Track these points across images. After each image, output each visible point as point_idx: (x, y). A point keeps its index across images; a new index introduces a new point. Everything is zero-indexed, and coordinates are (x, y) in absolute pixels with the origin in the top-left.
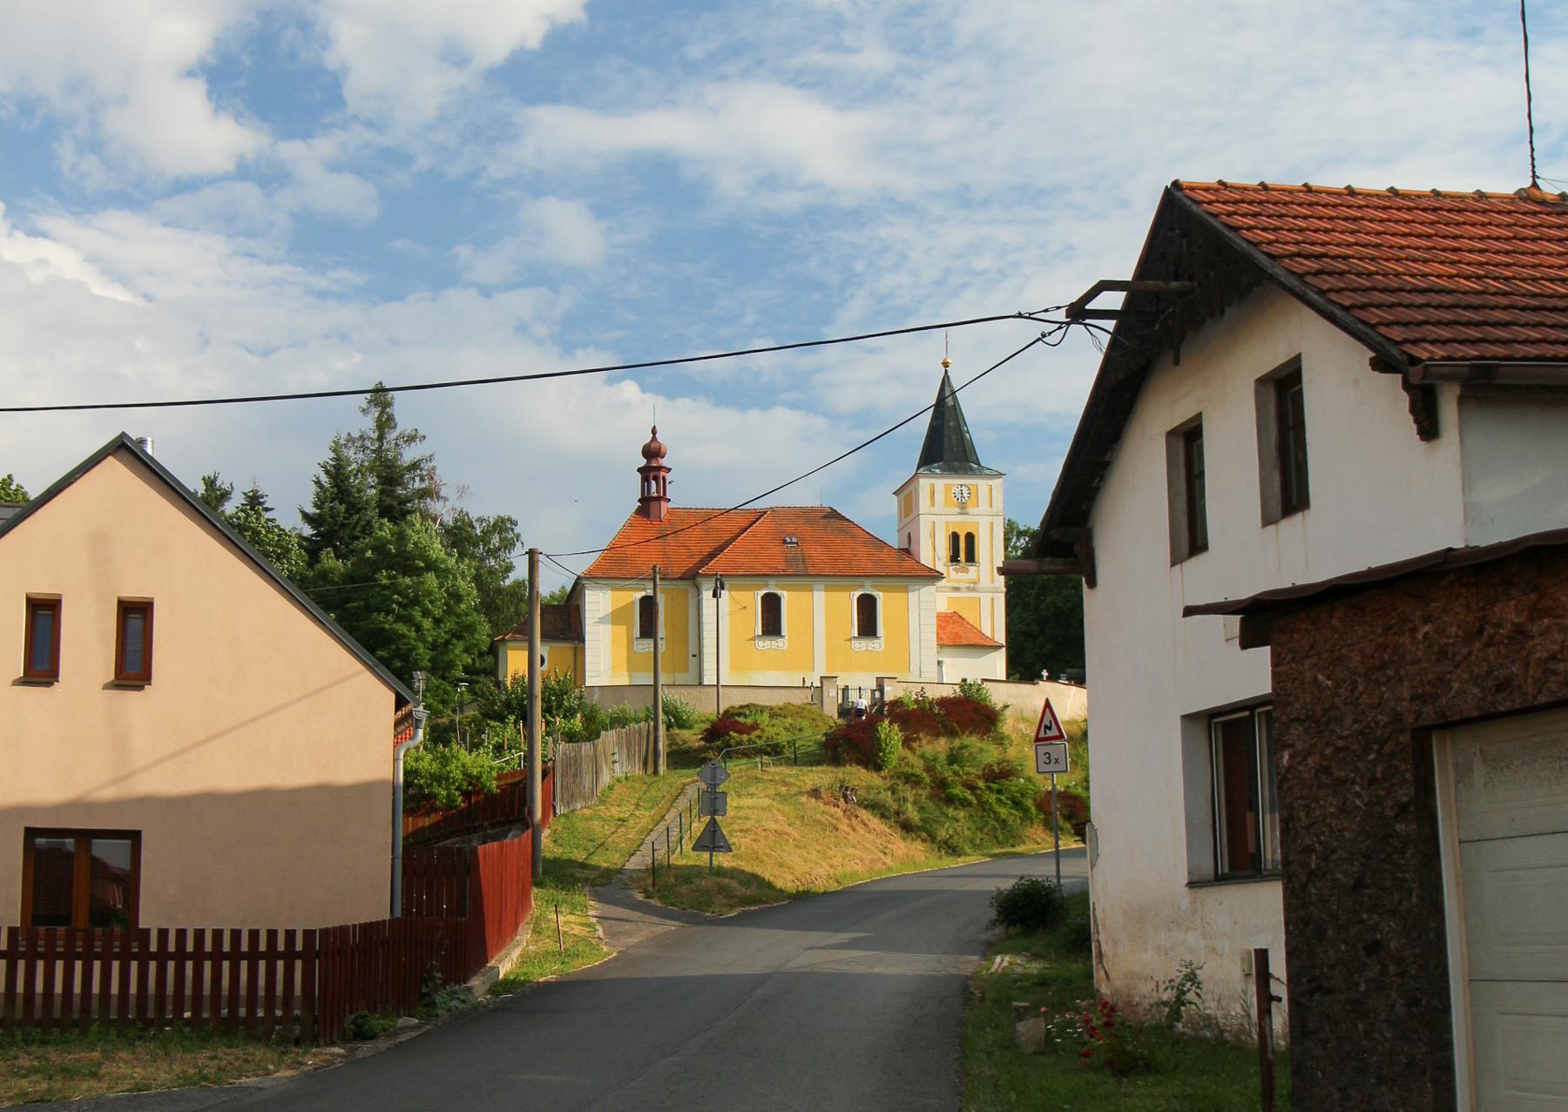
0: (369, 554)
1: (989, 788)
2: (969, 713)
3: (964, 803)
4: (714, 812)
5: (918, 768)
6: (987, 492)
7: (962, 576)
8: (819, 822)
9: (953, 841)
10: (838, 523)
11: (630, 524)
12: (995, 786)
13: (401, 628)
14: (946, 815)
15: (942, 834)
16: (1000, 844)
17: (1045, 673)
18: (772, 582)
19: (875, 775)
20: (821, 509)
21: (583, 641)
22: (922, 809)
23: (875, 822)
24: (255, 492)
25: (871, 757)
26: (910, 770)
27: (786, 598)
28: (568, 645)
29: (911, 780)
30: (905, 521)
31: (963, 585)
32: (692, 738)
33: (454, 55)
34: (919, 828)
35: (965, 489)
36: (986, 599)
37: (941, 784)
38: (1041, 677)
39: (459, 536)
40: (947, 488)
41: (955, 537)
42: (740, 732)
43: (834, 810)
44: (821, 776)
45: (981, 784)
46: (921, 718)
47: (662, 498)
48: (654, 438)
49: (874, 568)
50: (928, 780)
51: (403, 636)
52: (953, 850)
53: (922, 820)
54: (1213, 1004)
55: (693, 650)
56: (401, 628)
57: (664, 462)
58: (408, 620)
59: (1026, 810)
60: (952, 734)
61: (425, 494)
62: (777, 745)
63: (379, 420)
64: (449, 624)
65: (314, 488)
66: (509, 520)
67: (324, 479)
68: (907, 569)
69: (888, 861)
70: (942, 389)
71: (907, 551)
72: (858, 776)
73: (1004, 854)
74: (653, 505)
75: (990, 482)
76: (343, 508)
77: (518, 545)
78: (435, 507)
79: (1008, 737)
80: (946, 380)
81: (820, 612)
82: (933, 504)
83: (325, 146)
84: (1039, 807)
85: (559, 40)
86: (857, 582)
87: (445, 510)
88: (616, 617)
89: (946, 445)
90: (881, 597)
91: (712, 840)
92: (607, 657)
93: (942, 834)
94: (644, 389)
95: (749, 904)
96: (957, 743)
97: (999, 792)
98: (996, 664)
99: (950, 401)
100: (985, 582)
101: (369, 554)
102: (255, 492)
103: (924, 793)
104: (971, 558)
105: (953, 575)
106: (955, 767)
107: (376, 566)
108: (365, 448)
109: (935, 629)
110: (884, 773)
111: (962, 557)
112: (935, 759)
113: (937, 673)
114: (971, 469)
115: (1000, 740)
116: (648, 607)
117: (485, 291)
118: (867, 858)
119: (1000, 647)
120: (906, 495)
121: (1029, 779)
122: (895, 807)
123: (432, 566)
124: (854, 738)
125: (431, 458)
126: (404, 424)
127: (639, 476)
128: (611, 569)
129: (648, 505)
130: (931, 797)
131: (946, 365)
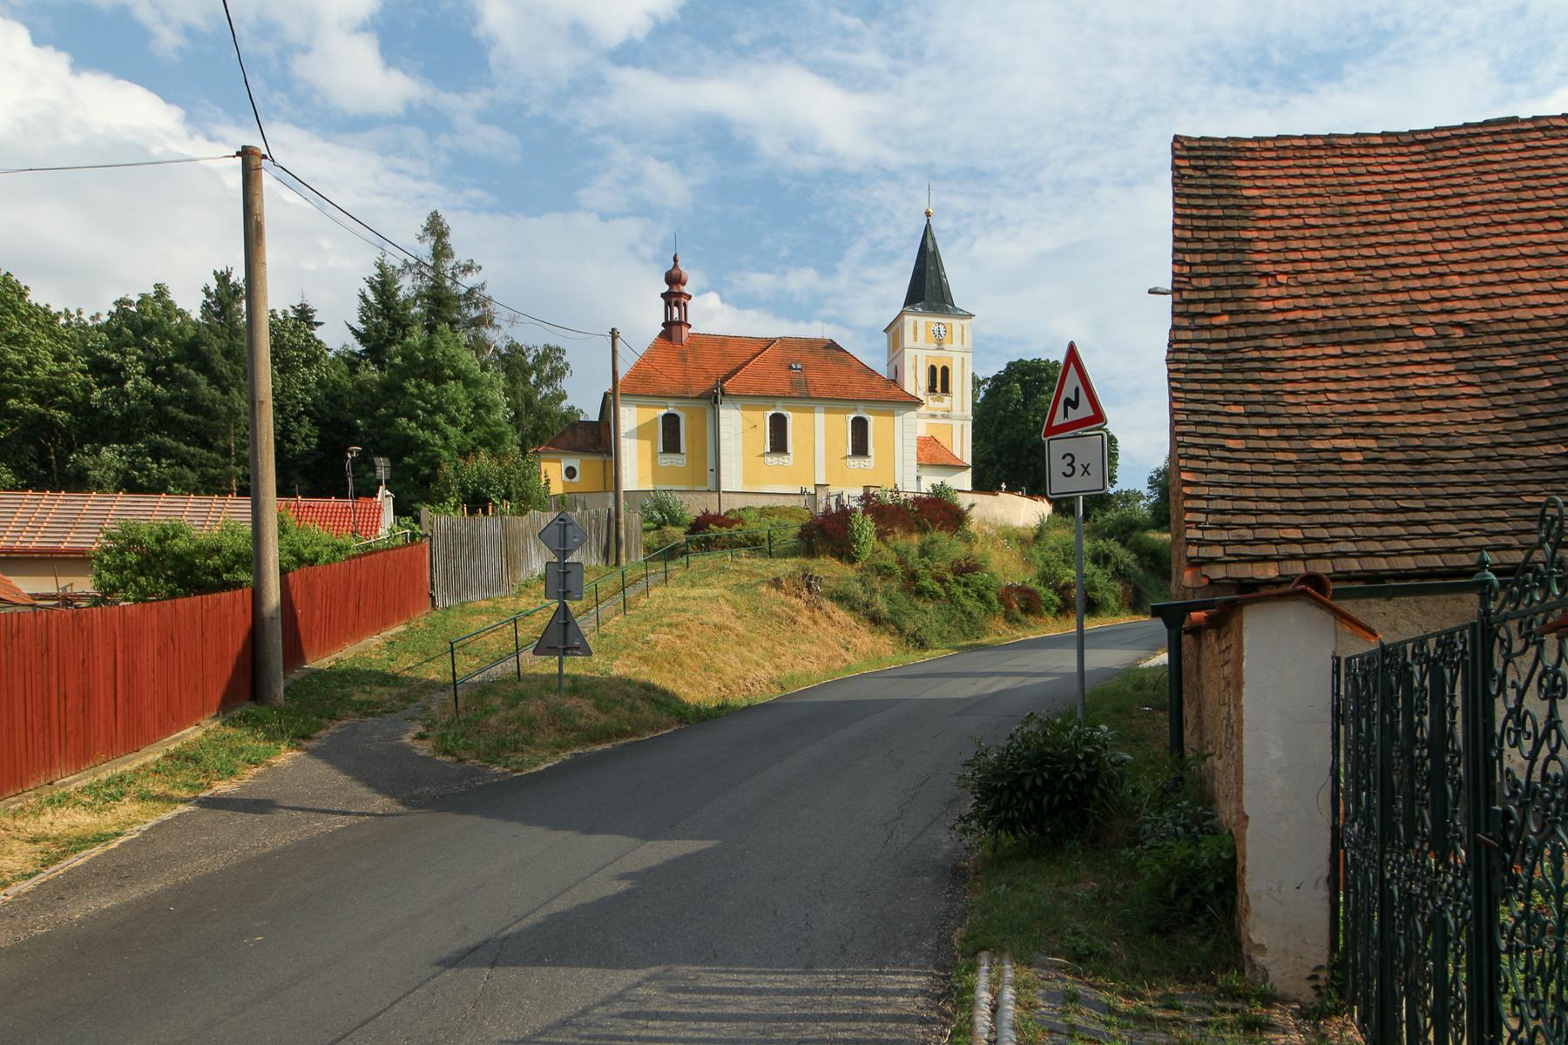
0: (398, 360)
1: (958, 582)
2: (938, 512)
3: (934, 596)
4: (565, 594)
5: (890, 559)
7: (938, 404)
8: (773, 614)
9: (922, 634)
10: (836, 353)
11: (655, 346)
12: (963, 580)
13: (424, 435)
14: (916, 608)
15: (910, 626)
18: (779, 403)
20: (822, 341)
22: (891, 600)
23: (840, 615)
24: (304, 306)
26: (882, 563)
27: (792, 418)
29: (884, 572)
31: (939, 413)
32: (678, 534)
33: (579, 33)
36: (957, 425)
37: (913, 577)
39: (512, 362)
40: (927, 324)
41: (933, 369)
42: (720, 526)
43: (794, 601)
44: (785, 567)
45: (950, 577)
46: (889, 514)
47: (682, 323)
48: (675, 266)
50: (899, 572)
51: (425, 442)
52: (922, 645)
55: (711, 464)
56: (424, 435)
57: (686, 289)
58: (434, 428)
59: (989, 603)
61: (478, 322)
62: (757, 538)
63: (434, 248)
64: (479, 432)
65: (357, 303)
66: (558, 349)
67: (371, 297)
69: (850, 657)
70: (925, 236)
72: (828, 568)
73: (970, 646)
76: (387, 323)
78: (490, 334)
79: (974, 535)
80: (928, 228)
81: (819, 432)
82: (915, 340)
83: (477, 100)
84: (1001, 600)
85: (661, 30)
86: (851, 405)
87: (497, 338)
88: (642, 432)
90: (872, 420)
91: (562, 637)
92: (637, 465)
93: (910, 626)
94: (723, 301)
95: (594, 741)
96: (928, 537)
97: (966, 585)
98: (964, 480)
99: (930, 246)
100: (956, 411)
101: (398, 360)
102: (304, 306)
103: (895, 585)
105: (931, 404)
106: (926, 559)
107: (404, 373)
108: (422, 275)
110: (859, 565)
113: (912, 481)
115: (968, 539)
116: (671, 422)
117: (604, 217)
118: (825, 655)
120: (894, 330)
121: (992, 575)
122: (865, 599)
123: (459, 376)
124: (827, 532)
125: (483, 287)
126: (461, 256)
128: (638, 386)
129: (671, 329)
130: (903, 590)
131: (928, 214)
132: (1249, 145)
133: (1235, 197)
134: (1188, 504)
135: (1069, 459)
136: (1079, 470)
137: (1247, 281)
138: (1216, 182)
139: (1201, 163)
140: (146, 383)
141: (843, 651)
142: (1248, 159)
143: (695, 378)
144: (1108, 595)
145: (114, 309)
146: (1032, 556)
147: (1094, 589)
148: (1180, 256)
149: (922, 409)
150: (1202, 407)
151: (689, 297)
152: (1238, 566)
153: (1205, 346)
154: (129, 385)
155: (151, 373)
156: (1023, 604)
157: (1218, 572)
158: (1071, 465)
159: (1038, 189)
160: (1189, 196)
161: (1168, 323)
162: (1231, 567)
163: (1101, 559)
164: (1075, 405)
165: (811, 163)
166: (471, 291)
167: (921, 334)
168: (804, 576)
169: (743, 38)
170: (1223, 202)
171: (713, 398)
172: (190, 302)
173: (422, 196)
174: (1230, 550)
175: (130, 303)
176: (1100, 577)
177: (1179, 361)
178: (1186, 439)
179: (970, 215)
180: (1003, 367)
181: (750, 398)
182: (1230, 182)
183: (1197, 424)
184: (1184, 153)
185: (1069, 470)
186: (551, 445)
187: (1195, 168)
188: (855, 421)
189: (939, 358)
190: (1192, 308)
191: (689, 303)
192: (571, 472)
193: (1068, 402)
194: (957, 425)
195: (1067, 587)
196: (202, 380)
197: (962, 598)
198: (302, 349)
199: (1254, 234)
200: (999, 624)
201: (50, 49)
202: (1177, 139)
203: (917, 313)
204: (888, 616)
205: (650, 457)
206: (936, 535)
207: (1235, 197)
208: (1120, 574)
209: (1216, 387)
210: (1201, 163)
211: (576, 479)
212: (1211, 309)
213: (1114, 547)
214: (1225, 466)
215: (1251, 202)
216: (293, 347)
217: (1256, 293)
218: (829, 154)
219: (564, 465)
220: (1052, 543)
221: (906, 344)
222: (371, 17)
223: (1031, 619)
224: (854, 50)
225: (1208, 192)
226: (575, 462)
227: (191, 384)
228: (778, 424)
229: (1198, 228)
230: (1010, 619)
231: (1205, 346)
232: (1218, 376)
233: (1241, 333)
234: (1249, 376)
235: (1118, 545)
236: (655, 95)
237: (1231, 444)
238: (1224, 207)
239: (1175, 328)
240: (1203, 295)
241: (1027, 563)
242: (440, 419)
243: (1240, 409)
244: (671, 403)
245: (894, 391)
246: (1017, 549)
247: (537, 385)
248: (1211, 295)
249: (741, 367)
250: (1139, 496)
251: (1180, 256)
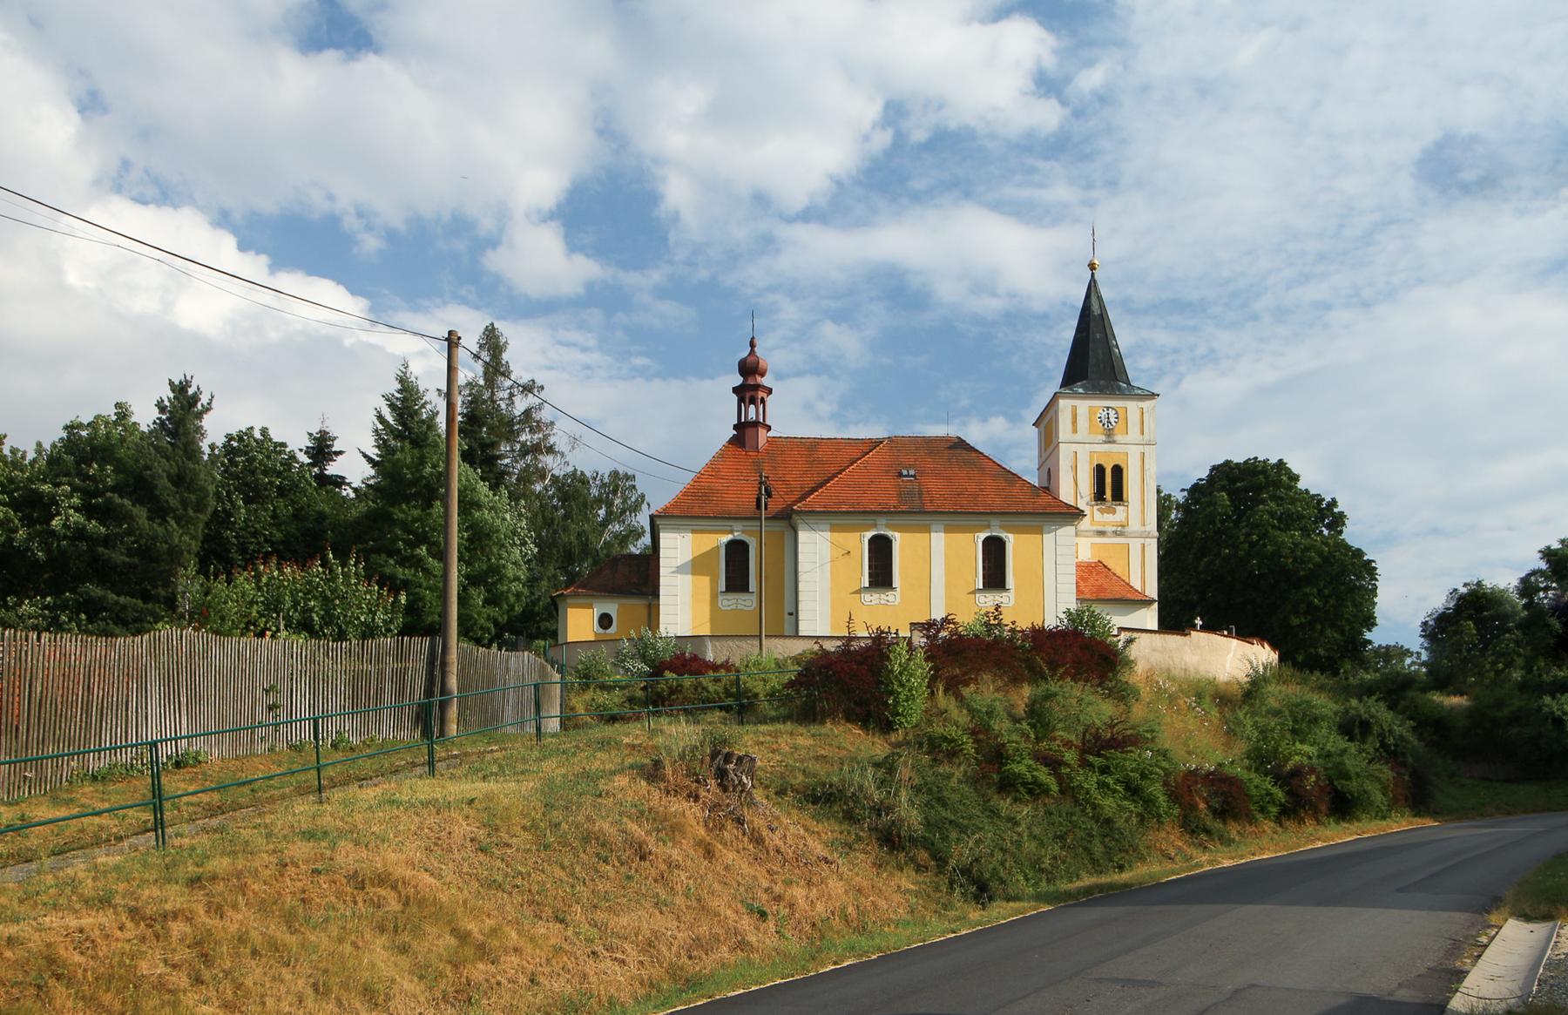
1: (1084, 763)
2: (1082, 652)
3: (1035, 790)
6: (1138, 458)
7: (1108, 517)
10: (966, 455)
11: (722, 455)
12: (1097, 761)
14: (994, 813)
16: (1097, 867)
17: (1199, 622)
19: (878, 740)
27: (898, 539)
29: (940, 749)
30: (1045, 456)
31: (1109, 529)
34: (913, 841)
35: (1112, 413)
36: (1135, 545)
37: (996, 756)
38: (1194, 627)
40: (1092, 410)
41: (1100, 470)
45: (1070, 756)
48: (752, 352)
49: (1004, 505)
52: (982, 892)
53: (928, 824)
57: (765, 381)
59: (1149, 802)
60: (1036, 676)
65: (370, 421)
68: (1045, 509)
70: (1088, 296)
71: (1047, 489)
72: (846, 746)
74: (749, 432)
75: (1141, 404)
77: (644, 506)
78: (548, 461)
80: (1092, 286)
82: (1075, 431)
83: (656, 276)
84: (1174, 796)
88: (698, 566)
89: (1092, 361)
90: (1011, 540)
92: (684, 606)
93: (961, 851)
97: (1104, 770)
98: (1149, 618)
100: (1134, 525)
104: (1118, 496)
105: (1095, 517)
109: (1073, 579)
110: (893, 738)
111: (1108, 494)
112: (990, 714)
114: (1119, 388)
115: (1123, 694)
116: (736, 553)
119: (1151, 602)
120: (1046, 422)
121: (1164, 754)
126: (520, 373)
127: (735, 398)
128: (692, 509)
130: (974, 781)
131: (1092, 267)
140: (76, 518)
141: (746, 923)
143: (765, 492)
144: (1368, 786)
145: (65, 435)
146: (1239, 723)
147: (1346, 776)
149: (1085, 524)
151: (770, 391)
154: (56, 522)
155: (88, 510)
156: (1218, 802)
159: (1255, 318)
163: (1353, 728)
165: (990, 306)
166: (527, 413)
167: (1083, 423)
168: (714, 756)
169: (918, 184)
171: (788, 519)
172: (145, 416)
173: (588, 367)
175: (80, 426)
176: (1355, 758)
179: (1175, 351)
180: (1204, 474)
181: (839, 516)
186: (583, 586)
188: (987, 542)
189: (1109, 454)
191: (769, 400)
192: (605, 621)
194: (1135, 545)
195: (1297, 772)
196: (141, 513)
197: (1095, 793)
198: (279, 474)
200: (1171, 838)
201: (252, 253)
203: (1076, 396)
204: (920, 830)
205: (708, 597)
206: (1053, 687)
208: (1391, 753)
211: (612, 630)
213: (1379, 712)
216: (265, 473)
218: (1012, 295)
219: (596, 612)
220: (1273, 703)
221: (1062, 437)
222: (558, 206)
223: (1233, 830)
224: (1041, 186)
226: (612, 608)
227: (129, 517)
228: (881, 552)
230: (1192, 827)
235: (1382, 706)
236: (830, 251)
241: (1231, 733)
242: (423, 551)
244: (738, 526)
245: (1045, 499)
246: (1215, 712)
247: (605, 524)
249: (834, 476)
250: (1408, 653)
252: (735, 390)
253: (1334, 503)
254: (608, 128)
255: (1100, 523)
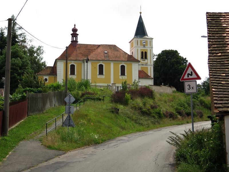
7: (144, 62)
17: (163, 84)
21: (56, 75)
25: (125, 103)
28: (53, 76)
31: (144, 64)
36: (149, 67)
39: (31, 51)
41: (142, 53)
47: (76, 41)
48: (75, 27)
54: (94, 117)
57: (77, 33)
98: (150, 82)
100: (149, 63)
104: (146, 58)
105: (142, 61)
111: (144, 57)
119: (206, 37)
132: (223, 14)
133: (221, 26)
134: (214, 95)
135: (189, 86)
136: (191, 88)
137: (225, 46)
138: (216, 23)
139: (213, 19)
142: (224, 18)
148: (209, 40)
150: (216, 74)
152: (225, 108)
153: (216, 60)
157: (221, 110)
158: (189, 87)
160: (210, 26)
161: (207, 55)
162: (223, 109)
164: (191, 75)
170: (218, 28)
174: (223, 105)
177: (210, 64)
178: (213, 81)
180: (161, 52)
182: (219, 23)
183: (215, 78)
184: (209, 16)
185: (189, 88)
187: (211, 20)
190: (213, 52)
193: (188, 74)
199: (226, 35)
202: (207, 13)
207: (221, 26)
209: (219, 70)
210: (213, 19)
211: (47, 82)
212: (217, 52)
214: (221, 87)
215: (225, 28)
217: (227, 48)
225: (215, 25)
229: (213, 34)
231: (216, 60)
232: (219, 67)
233: (223, 57)
234: (226, 67)
237: (223, 82)
238: (218, 29)
239: (209, 56)
240: (215, 49)
243: (224, 75)
248: (217, 49)
251: (209, 40)
252: (71, 34)
253: (186, 58)
254: (154, 100)
255: (142, 63)
